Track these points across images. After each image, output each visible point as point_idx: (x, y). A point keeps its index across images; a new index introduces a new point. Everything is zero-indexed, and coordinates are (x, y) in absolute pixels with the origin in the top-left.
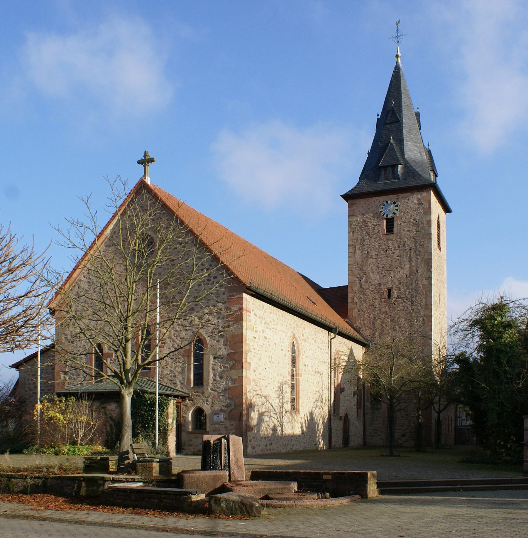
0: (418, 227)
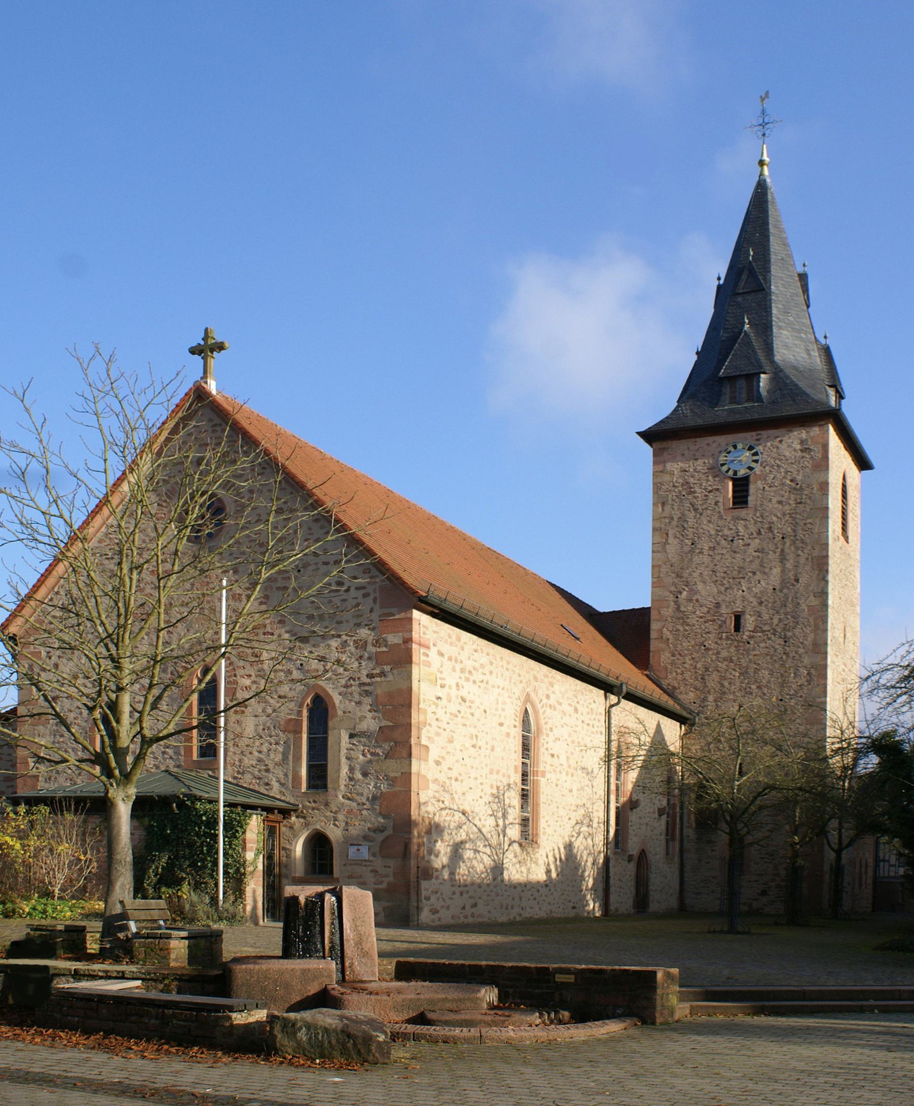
0: (801, 495)
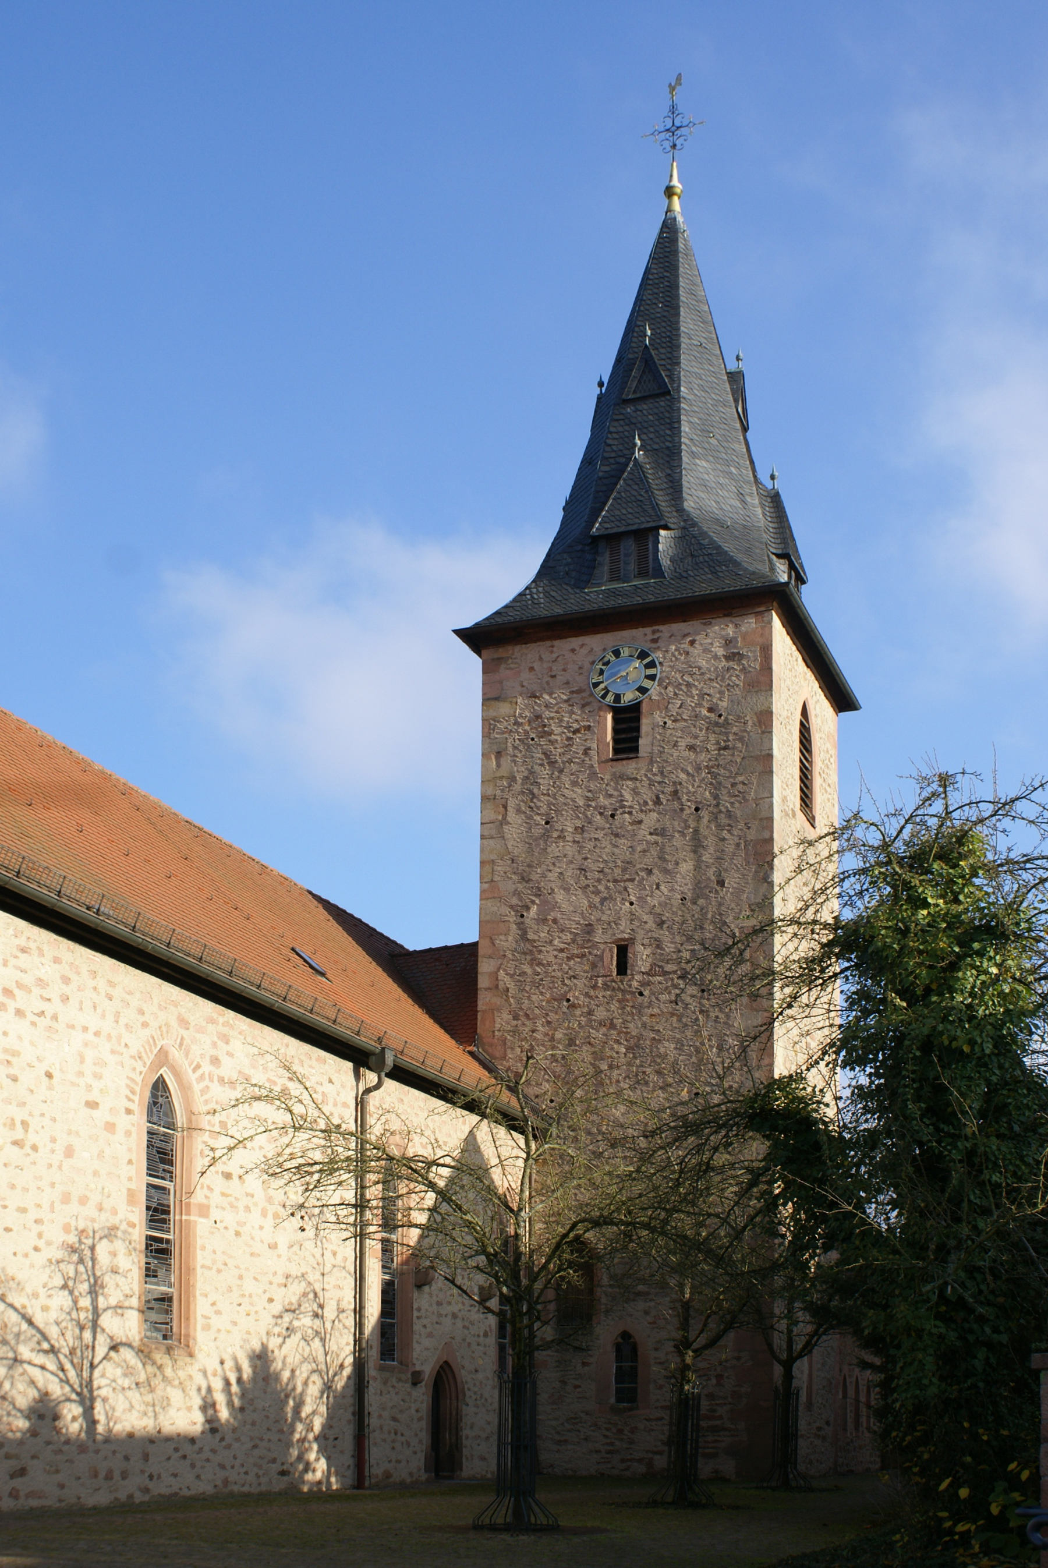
0: (727, 734)
